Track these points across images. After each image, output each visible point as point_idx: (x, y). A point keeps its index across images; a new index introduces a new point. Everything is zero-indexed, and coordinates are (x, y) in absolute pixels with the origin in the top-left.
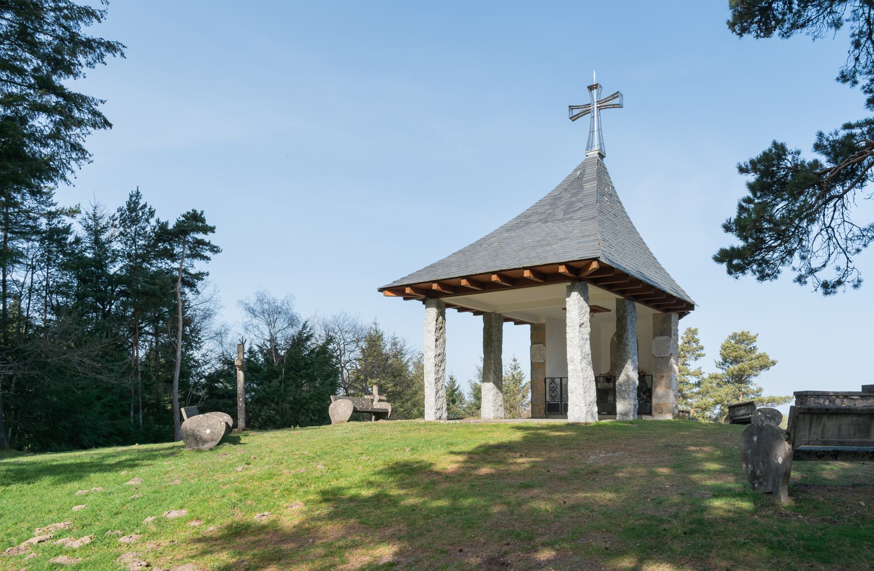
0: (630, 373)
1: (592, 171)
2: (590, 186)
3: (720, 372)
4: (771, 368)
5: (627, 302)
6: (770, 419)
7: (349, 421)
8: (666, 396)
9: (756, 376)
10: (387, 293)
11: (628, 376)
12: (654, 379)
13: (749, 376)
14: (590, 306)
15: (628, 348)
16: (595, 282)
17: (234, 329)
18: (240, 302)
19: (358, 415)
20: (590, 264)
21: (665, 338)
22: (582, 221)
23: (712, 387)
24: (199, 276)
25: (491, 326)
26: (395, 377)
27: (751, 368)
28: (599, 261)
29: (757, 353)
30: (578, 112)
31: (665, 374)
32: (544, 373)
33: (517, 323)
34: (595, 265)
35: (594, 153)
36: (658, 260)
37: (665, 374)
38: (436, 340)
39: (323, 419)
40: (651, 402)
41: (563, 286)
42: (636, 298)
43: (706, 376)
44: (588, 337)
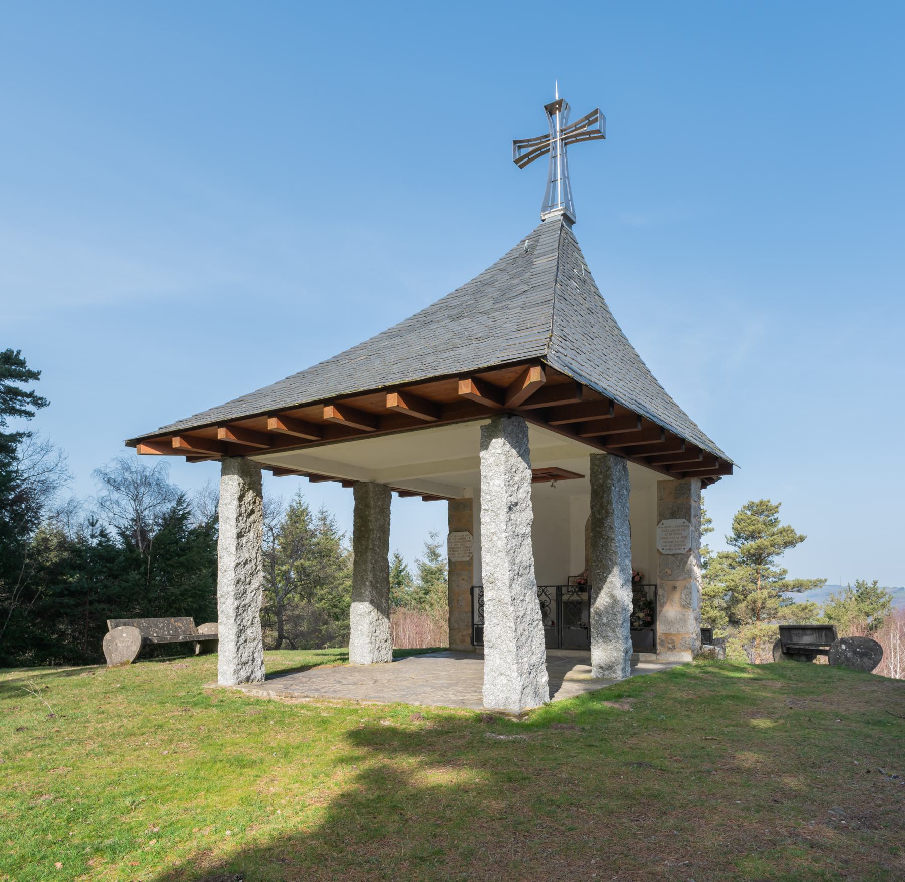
0: (615, 592)
1: (551, 240)
2: (545, 262)
3: (731, 549)
4: (798, 545)
5: (612, 460)
6: (862, 655)
7: (134, 662)
8: (684, 620)
9: (778, 554)
10: (144, 448)
11: (613, 597)
12: (660, 591)
13: (769, 555)
14: (533, 471)
15: (614, 546)
16: (545, 418)
17: (86, 506)
18: (98, 472)
19: (149, 651)
20: (526, 373)
21: (680, 521)
22: (523, 309)
23: (722, 570)
24: (16, 437)
25: (367, 506)
26: (322, 557)
27: (772, 546)
28: (544, 367)
29: (780, 526)
30: (529, 152)
31: (678, 584)
32: (471, 578)
33: (427, 498)
34: (535, 375)
35: (555, 214)
36: (667, 390)
37: (678, 584)
38: (240, 536)
39: (91, 655)
40: (654, 631)
41: (473, 428)
42: (629, 453)
43: (714, 555)
44: (529, 529)
